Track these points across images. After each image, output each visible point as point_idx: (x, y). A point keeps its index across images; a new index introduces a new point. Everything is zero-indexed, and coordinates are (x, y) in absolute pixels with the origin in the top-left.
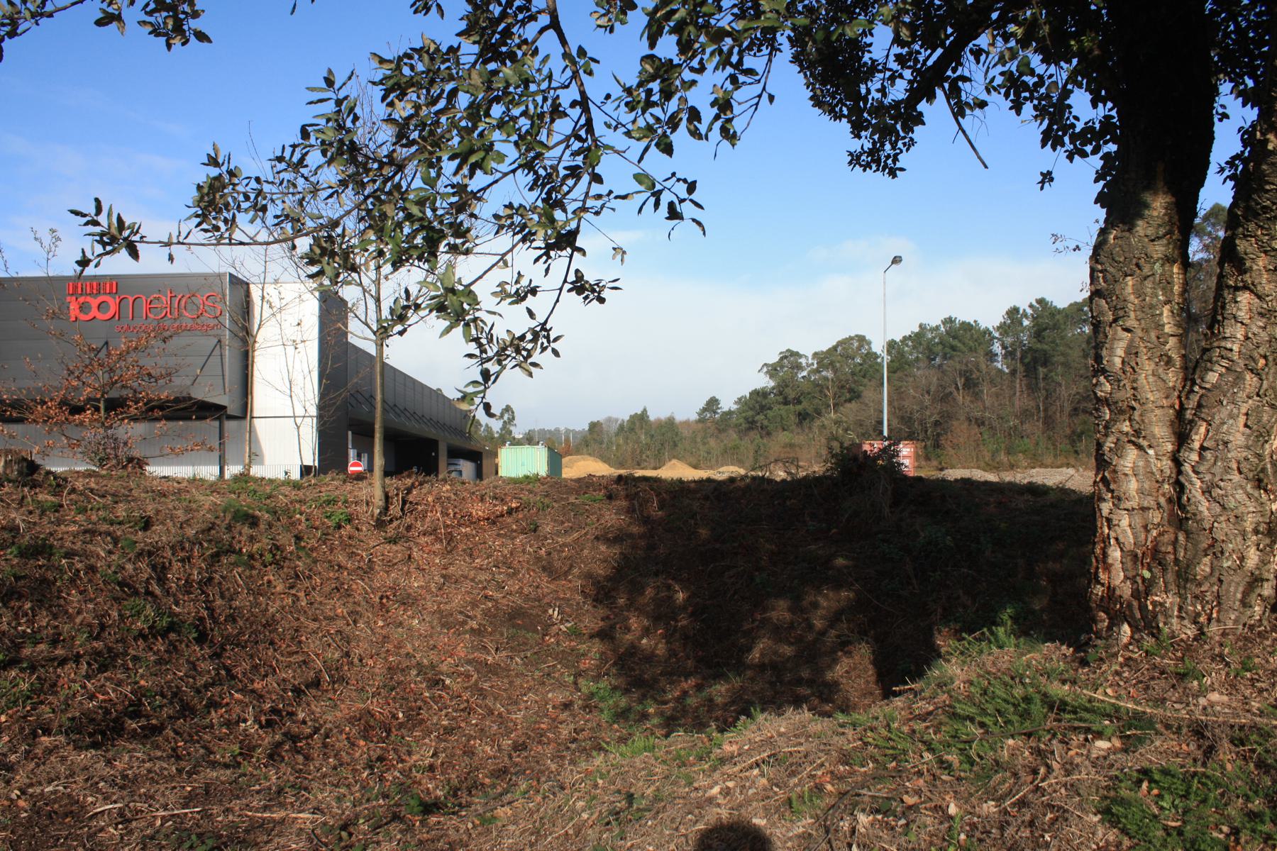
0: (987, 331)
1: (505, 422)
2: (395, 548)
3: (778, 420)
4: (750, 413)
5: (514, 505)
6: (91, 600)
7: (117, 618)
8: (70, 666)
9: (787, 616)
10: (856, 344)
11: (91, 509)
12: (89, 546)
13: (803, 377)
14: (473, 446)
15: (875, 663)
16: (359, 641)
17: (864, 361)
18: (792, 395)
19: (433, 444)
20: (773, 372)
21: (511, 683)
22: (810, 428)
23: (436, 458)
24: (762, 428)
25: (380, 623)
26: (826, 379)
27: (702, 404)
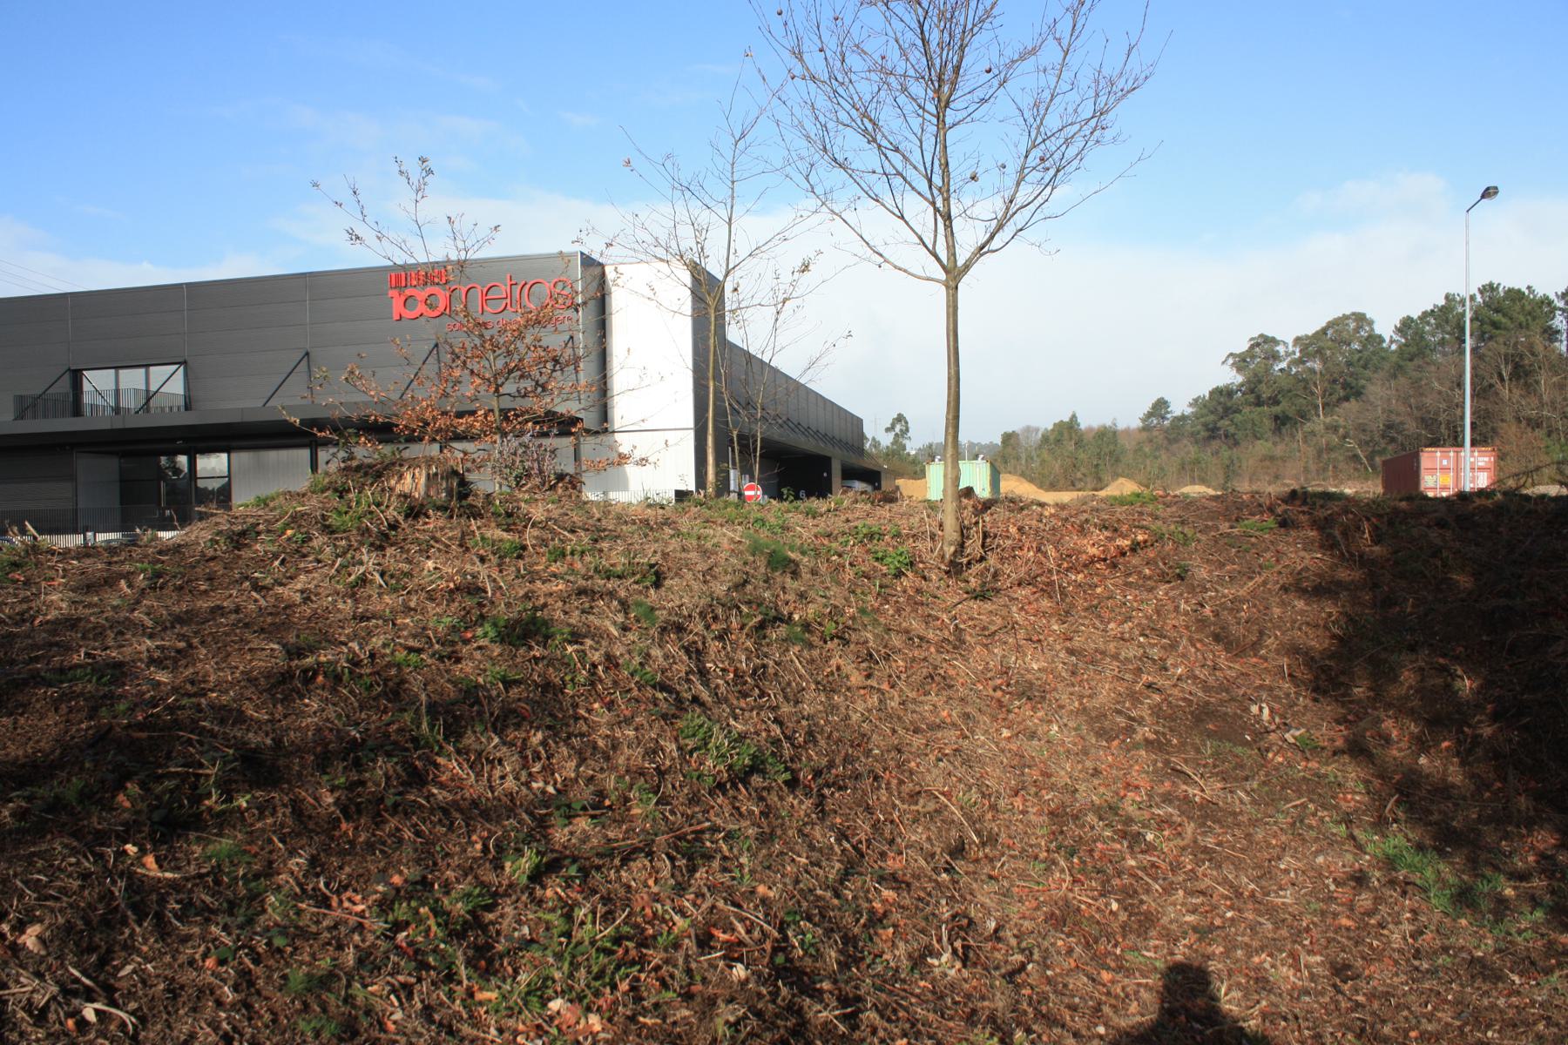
0: (1546, 301)
1: (896, 435)
2: (988, 606)
4: (1212, 418)
5: (1140, 538)
6: (628, 721)
7: (675, 754)
8: (641, 862)
10: (1353, 325)
11: (572, 553)
12: (591, 617)
13: (1281, 370)
14: (867, 463)
17: (1364, 346)
18: (1266, 393)
19: (824, 462)
20: (1242, 364)
21: (1248, 836)
22: (1293, 436)
23: (829, 479)
24: (1226, 436)
25: (1006, 733)
26: (1312, 371)
27: (1147, 407)
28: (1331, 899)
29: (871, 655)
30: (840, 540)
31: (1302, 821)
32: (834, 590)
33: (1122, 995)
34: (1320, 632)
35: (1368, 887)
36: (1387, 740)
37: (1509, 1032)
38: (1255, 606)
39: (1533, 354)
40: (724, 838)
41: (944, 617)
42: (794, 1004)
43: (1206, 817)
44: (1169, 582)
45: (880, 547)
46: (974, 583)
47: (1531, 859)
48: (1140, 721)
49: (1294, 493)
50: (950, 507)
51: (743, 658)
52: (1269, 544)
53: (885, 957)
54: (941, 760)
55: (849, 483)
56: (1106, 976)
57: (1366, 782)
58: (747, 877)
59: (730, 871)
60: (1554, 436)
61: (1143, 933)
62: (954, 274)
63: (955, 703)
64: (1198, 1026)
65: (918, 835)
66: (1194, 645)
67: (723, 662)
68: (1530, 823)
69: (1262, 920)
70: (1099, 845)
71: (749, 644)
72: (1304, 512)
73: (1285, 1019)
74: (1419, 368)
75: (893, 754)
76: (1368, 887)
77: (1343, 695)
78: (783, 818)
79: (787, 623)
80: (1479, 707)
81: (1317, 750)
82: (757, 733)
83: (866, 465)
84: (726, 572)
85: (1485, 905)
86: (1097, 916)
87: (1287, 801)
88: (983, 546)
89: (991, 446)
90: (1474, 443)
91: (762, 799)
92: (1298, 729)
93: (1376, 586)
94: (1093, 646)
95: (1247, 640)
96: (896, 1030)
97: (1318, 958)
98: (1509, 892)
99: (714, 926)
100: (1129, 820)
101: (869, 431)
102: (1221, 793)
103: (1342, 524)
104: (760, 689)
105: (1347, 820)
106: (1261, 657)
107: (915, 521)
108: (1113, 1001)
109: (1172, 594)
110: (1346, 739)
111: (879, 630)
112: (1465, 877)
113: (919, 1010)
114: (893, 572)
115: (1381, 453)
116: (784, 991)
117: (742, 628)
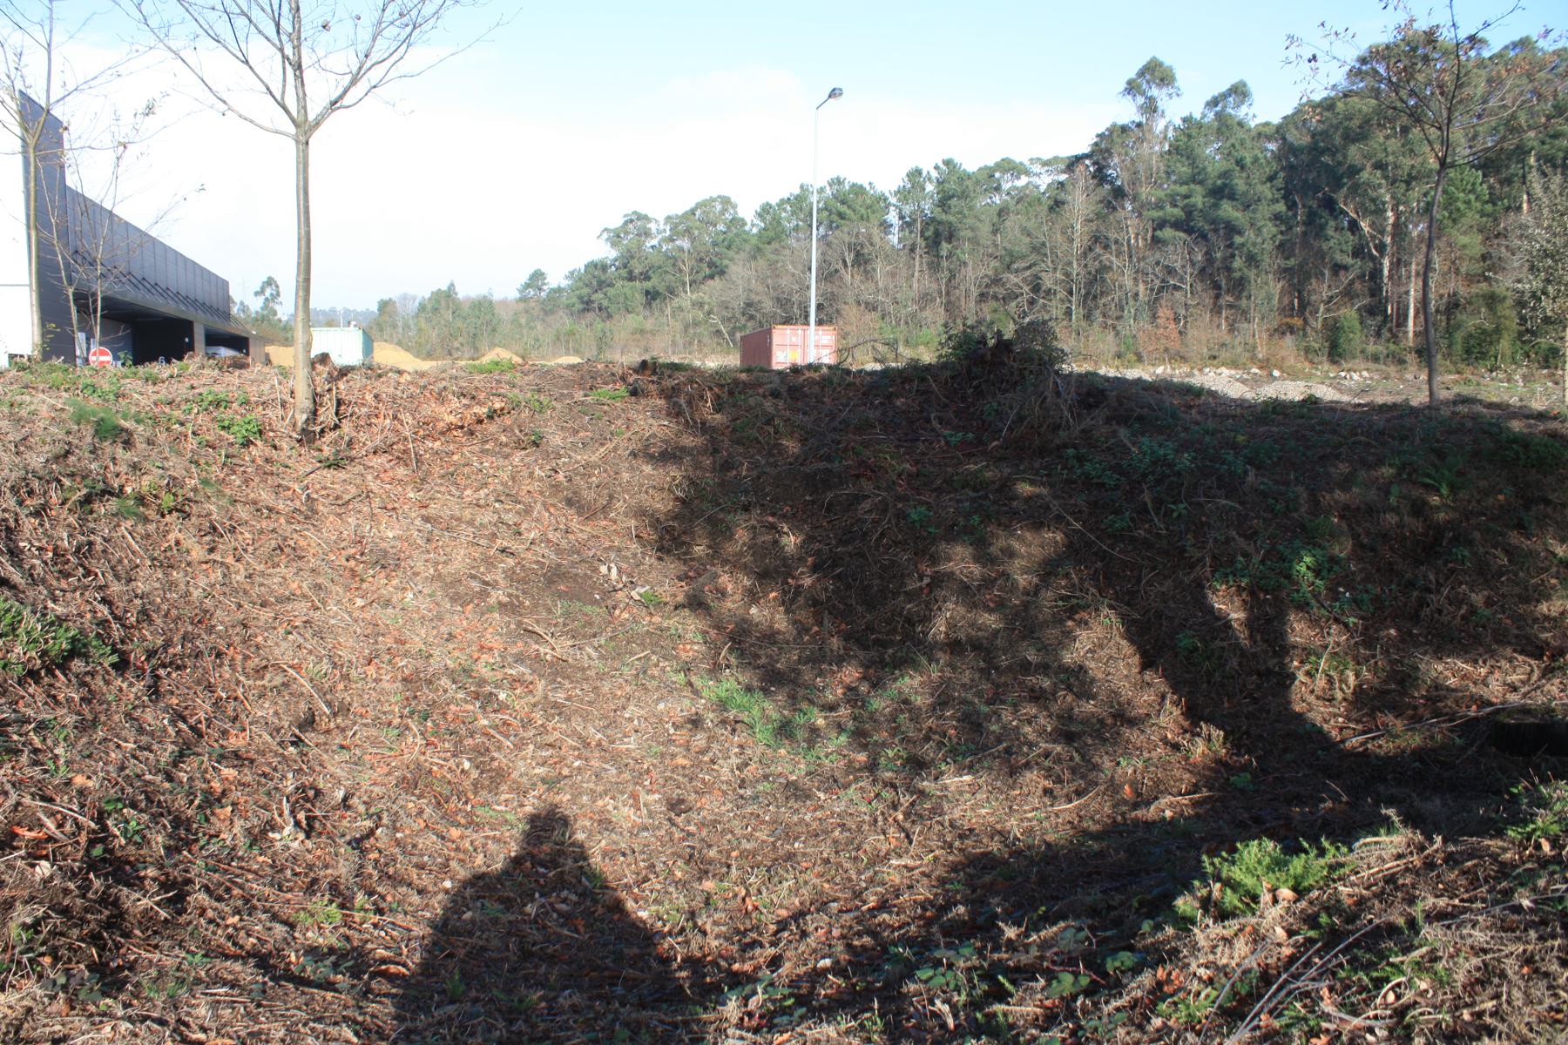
1: (267, 299)
2: (342, 475)
3: (622, 299)
5: (497, 406)
9: (976, 569)
10: (719, 207)
13: (653, 247)
15: (1130, 636)
16: (337, 634)
17: (729, 228)
18: (638, 269)
19: (186, 327)
22: (662, 311)
24: (600, 309)
25: (360, 602)
26: (681, 249)
28: (671, 741)
29: (215, 529)
30: (184, 407)
31: (645, 672)
32: (174, 460)
33: (471, 849)
34: (666, 494)
35: (703, 728)
36: (722, 593)
37: (812, 842)
38: (605, 471)
39: (871, 244)
40: (34, 729)
41: (296, 487)
42: (110, 896)
43: (557, 674)
44: (524, 449)
45: (226, 415)
46: (327, 451)
47: (840, 691)
48: (494, 585)
49: (644, 363)
50: (302, 373)
51: (65, 535)
52: (620, 412)
53: (222, 836)
54: (290, 633)
55: (212, 350)
56: (455, 833)
57: (704, 633)
58: (63, 768)
59: (42, 764)
60: (887, 318)
61: (494, 788)
62: (304, 129)
63: (305, 574)
64: (542, 870)
65: (265, 710)
66: (548, 510)
67: (40, 540)
68: (840, 661)
70: (453, 707)
71: (71, 519)
72: (653, 382)
73: (624, 854)
74: (776, 252)
75: (238, 629)
76: (703, 728)
77: (685, 554)
78: (109, 704)
79: (118, 497)
80: (801, 560)
81: (660, 605)
82: (81, 615)
83: (233, 331)
84: (44, 443)
85: (801, 735)
86: (449, 776)
87: (632, 654)
88: (337, 414)
89: (367, 313)
90: (820, 323)
91: (83, 684)
92: (643, 586)
93: (716, 451)
94: (448, 512)
95: (598, 504)
96: (227, 909)
97: (657, 796)
98: (820, 722)
99: (18, 824)
100: (482, 682)
101: (236, 293)
102: (571, 651)
104: (85, 568)
106: (611, 520)
107: (265, 388)
108: (461, 856)
109: (527, 460)
110: (687, 595)
111: (224, 502)
112: (786, 712)
113: (255, 886)
114: (241, 441)
116: (98, 884)
117: (63, 504)
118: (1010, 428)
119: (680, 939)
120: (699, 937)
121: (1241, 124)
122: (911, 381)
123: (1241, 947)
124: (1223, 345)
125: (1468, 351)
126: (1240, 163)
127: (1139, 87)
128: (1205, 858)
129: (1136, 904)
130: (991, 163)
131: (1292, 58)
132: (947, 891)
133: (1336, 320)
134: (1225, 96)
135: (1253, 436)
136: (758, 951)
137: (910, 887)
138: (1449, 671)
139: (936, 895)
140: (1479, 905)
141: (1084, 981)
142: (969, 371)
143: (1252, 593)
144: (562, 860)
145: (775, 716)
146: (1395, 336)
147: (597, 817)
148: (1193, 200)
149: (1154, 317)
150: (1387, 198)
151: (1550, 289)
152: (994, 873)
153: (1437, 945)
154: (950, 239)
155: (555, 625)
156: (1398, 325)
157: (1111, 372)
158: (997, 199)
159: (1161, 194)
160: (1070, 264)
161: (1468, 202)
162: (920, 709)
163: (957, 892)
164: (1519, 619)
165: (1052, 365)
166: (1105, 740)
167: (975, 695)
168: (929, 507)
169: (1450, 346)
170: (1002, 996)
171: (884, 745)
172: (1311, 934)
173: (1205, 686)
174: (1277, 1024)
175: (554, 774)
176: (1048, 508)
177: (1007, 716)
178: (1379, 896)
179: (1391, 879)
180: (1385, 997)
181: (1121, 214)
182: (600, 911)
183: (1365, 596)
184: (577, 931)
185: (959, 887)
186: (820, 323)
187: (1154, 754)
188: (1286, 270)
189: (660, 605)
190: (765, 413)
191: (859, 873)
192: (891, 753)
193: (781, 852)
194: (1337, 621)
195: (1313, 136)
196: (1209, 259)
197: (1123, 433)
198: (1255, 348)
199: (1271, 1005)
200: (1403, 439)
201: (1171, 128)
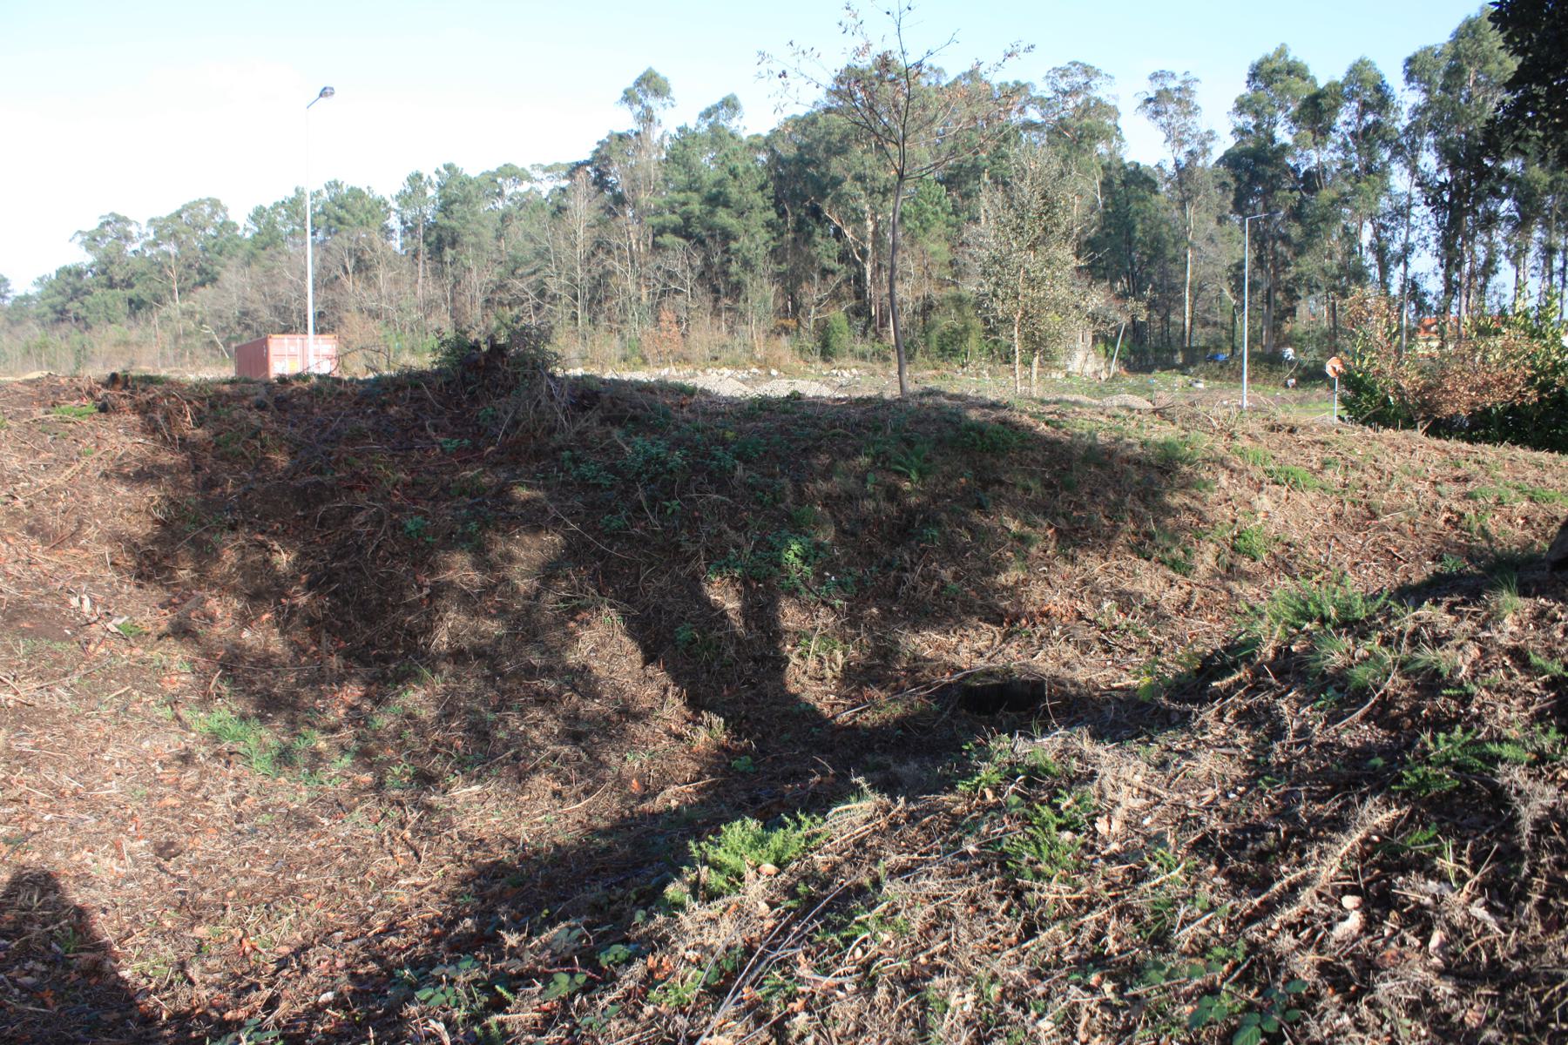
0: (382, 203)
3: (102, 308)
9: (476, 577)
10: (207, 210)
15: (631, 633)
21: (69, 734)
22: (148, 321)
24: (77, 319)
26: (168, 255)
34: (143, 517)
36: (212, 619)
47: (341, 711)
49: (114, 377)
68: (341, 680)
69: (85, 816)
73: (105, 911)
77: (168, 579)
80: (295, 578)
81: (141, 636)
87: (110, 691)
93: (198, 468)
97: (143, 843)
98: (322, 745)
103: (163, 408)
105: (173, 702)
106: (82, 548)
110: (171, 624)
112: (285, 739)
115: (236, 339)
118: (506, 434)
119: (167, 995)
120: (187, 991)
121: (732, 136)
122: (405, 388)
123: (726, 924)
124: (724, 346)
125: (943, 349)
126: (733, 173)
127: (634, 96)
128: (691, 843)
129: (634, 897)
130: (493, 169)
131: (764, 73)
132: (457, 905)
133: (826, 322)
134: (716, 108)
135: (741, 432)
136: (254, 994)
137: (419, 906)
138: (924, 643)
139: (445, 910)
140: (934, 856)
141: (581, 979)
142: (463, 377)
143: (745, 583)
144: (27, 928)
145: (273, 743)
146: (878, 335)
147: (73, 873)
148: (690, 207)
149: (658, 320)
150: (867, 208)
151: (999, 292)
152: (503, 881)
153: (896, 898)
154: (453, 244)
155: (18, 667)
156: (882, 325)
157: (608, 375)
158: (500, 205)
159: (660, 201)
160: (573, 269)
161: (935, 213)
162: (425, 722)
163: (467, 905)
164: (982, 591)
165: (546, 368)
166: (612, 737)
167: (481, 703)
168: (426, 516)
169: (927, 344)
170: (499, 1005)
171: (390, 762)
172: (792, 904)
173: (704, 676)
174: (758, 994)
175: (19, 832)
176: (545, 511)
177: (514, 722)
178: (850, 860)
179: (860, 843)
180: (853, 953)
181: (621, 220)
182: (74, 976)
183: (849, 579)
184: (44, 1005)
185: (469, 899)
186: (320, 331)
187: (659, 746)
188: (779, 275)
189: (141, 636)
190: (250, 426)
191: (366, 897)
192: (397, 771)
193: (282, 886)
194: (824, 604)
195: (799, 148)
196: (708, 265)
197: (617, 433)
198: (753, 348)
199: (753, 977)
200: (877, 429)
201: (667, 138)
